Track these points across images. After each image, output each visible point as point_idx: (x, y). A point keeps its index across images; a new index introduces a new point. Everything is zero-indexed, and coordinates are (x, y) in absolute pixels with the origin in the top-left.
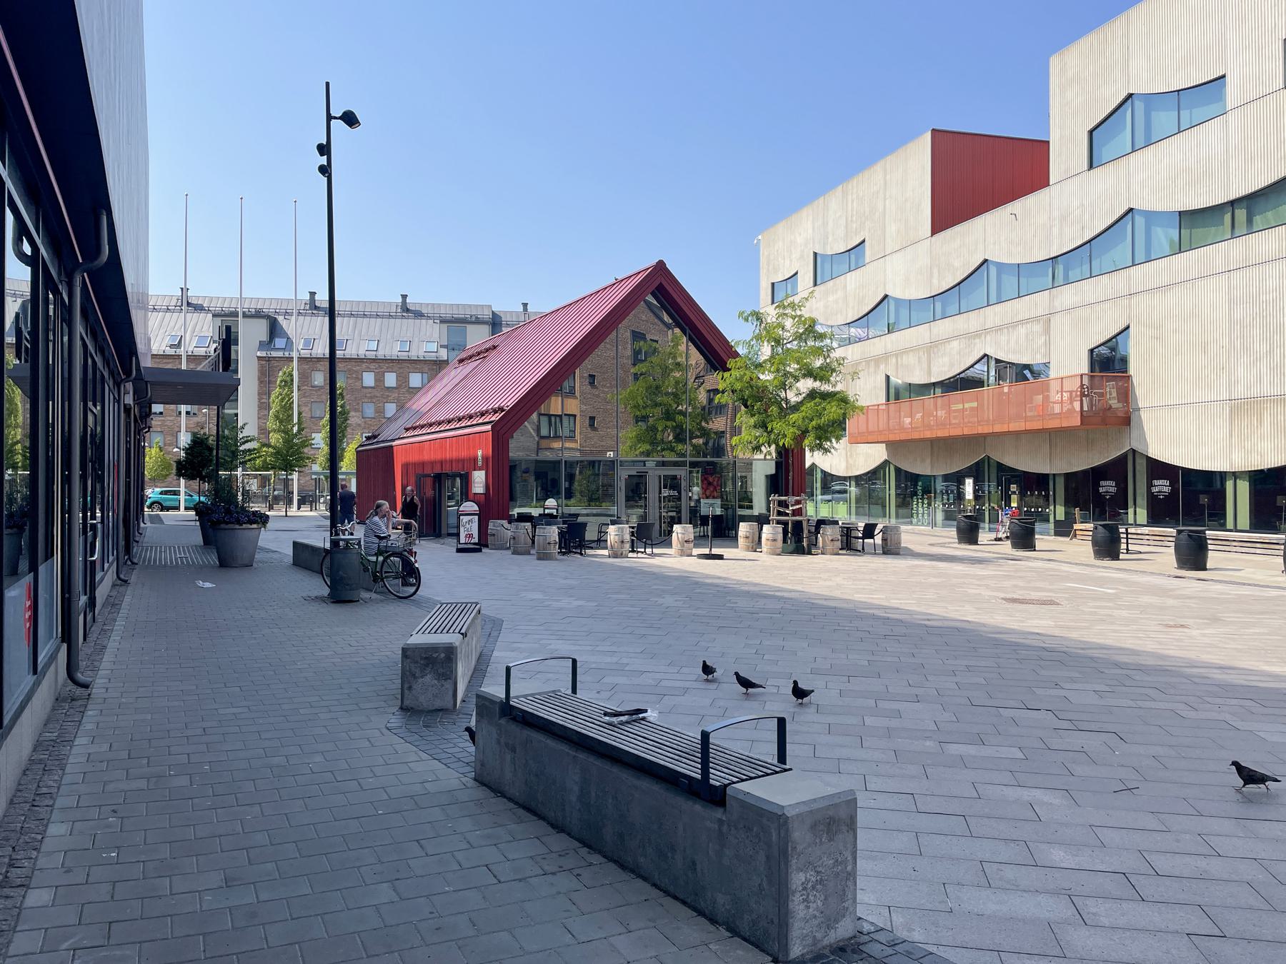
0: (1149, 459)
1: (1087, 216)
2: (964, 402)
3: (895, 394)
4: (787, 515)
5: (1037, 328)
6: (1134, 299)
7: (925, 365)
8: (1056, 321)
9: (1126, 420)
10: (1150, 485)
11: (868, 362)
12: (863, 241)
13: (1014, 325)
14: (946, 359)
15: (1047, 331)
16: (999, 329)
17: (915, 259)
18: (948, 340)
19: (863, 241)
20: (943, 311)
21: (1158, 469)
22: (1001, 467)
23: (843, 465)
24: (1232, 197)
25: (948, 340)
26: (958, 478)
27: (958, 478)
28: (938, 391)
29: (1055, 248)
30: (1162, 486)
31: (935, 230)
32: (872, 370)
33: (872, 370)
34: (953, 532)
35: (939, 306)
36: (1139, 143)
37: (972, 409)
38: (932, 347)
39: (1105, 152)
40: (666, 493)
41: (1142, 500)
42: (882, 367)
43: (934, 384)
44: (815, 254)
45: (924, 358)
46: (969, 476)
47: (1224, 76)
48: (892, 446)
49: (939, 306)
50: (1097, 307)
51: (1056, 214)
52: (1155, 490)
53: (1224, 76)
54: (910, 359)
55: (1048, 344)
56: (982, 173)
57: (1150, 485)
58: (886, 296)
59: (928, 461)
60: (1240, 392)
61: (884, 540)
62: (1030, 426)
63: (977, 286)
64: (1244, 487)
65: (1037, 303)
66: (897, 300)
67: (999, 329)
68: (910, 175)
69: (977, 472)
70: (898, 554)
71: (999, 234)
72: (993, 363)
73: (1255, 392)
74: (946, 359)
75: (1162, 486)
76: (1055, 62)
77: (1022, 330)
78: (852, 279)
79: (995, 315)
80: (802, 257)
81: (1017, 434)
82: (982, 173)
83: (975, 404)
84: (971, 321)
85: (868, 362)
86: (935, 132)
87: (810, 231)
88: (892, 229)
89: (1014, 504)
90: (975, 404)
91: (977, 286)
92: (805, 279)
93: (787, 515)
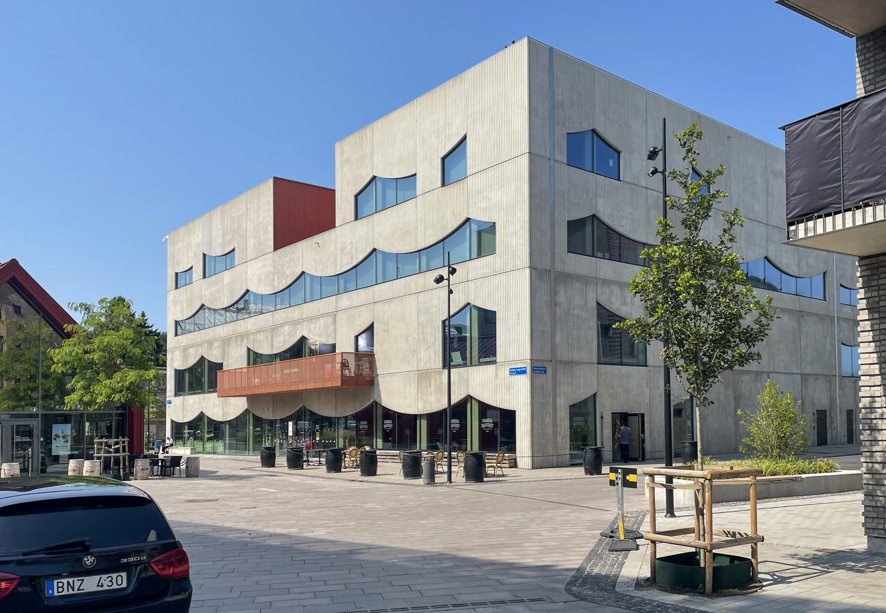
0: (384, 408)
1: (354, 251)
2: (293, 368)
3: (255, 358)
4: (110, 452)
5: (330, 320)
6: (377, 305)
7: (270, 340)
8: (340, 315)
9: (370, 382)
10: (480, 422)
11: (236, 338)
12: (234, 250)
13: (318, 317)
14: (281, 338)
15: (335, 322)
16: (310, 319)
17: (263, 268)
18: (282, 325)
19: (234, 250)
20: (345, 287)
21: (388, 414)
22: (312, 414)
23: (221, 412)
24: (419, 248)
25: (282, 325)
26: (284, 421)
27: (284, 421)
28: (278, 359)
29: (338, 268)
30: (388, 424)
31: (276, 248)
32: (239, 342)
33: (239, 342)
34: (258, 458)
35: (342, 282)
36: (379, 209)
37: (294, 373)
38: (274, 329)
39: (364, 210)
40: (18, 439)
41: (380, 434)
42: (245, 341)
43: (276, 355)
44: (204, 255)
45: (269, 336)
46: (290, 420)
47: (415, 175)
48: (252, 399)
49: (424, 259)
50: (359, 309)
51: (339, 246)
52: (483, 426)
53: (415, 175)
54: (261, 337)
55: (335, 331)
56: (302, 212)
57: (383, 424)
58: (375, 250)
59: (271, 409)
60: (422, 366)
61: (187, 467)
62: (319, 385)
63: (299, 288)
64: (424, 423)
65: (327, 304)
66: (384, 254)
67: (310, 319)
68: (259, 209)
69: (297, 417)
70: (197, 476)
71: (316, 255)
72: (475, 313)
73: (428, 366)
74: (281, 338)
75: (388, 424)
76: (338, 146)
77: (322, 321)
78: (227, 275)
79: (308, 309)
80: (195, 255)
81: (319, 390)
82: (302, 212)
83: (296, 370)
84: (295, 313)
85: (236, 338)
86: (275, 178)
87: (201, 237)
88: (251, 242)
89: (318, 439)
90: (296, 370)
91: (299, 288)
92: (198, 272)
93: (110, 452)
